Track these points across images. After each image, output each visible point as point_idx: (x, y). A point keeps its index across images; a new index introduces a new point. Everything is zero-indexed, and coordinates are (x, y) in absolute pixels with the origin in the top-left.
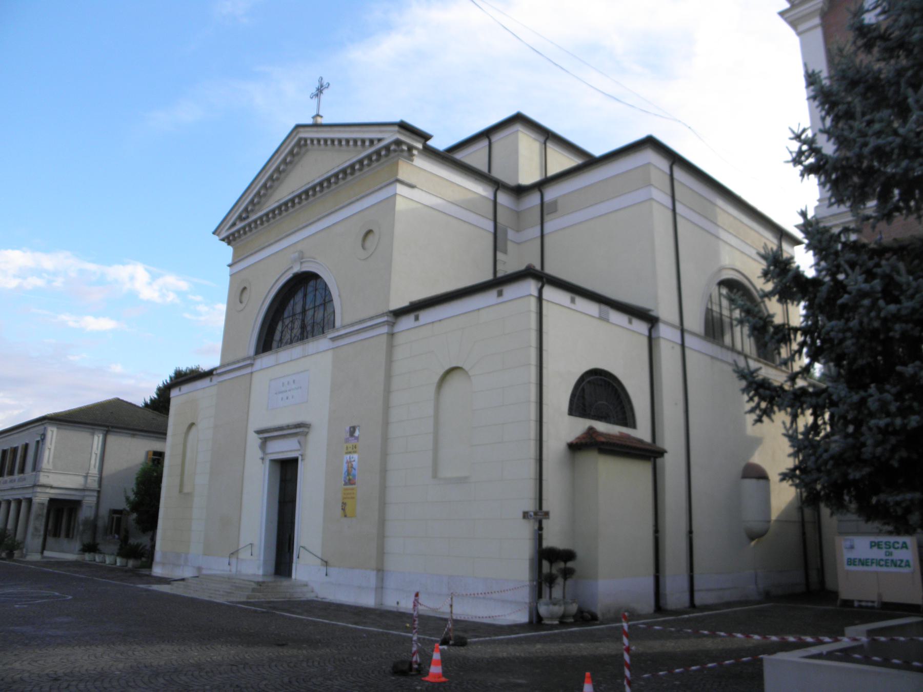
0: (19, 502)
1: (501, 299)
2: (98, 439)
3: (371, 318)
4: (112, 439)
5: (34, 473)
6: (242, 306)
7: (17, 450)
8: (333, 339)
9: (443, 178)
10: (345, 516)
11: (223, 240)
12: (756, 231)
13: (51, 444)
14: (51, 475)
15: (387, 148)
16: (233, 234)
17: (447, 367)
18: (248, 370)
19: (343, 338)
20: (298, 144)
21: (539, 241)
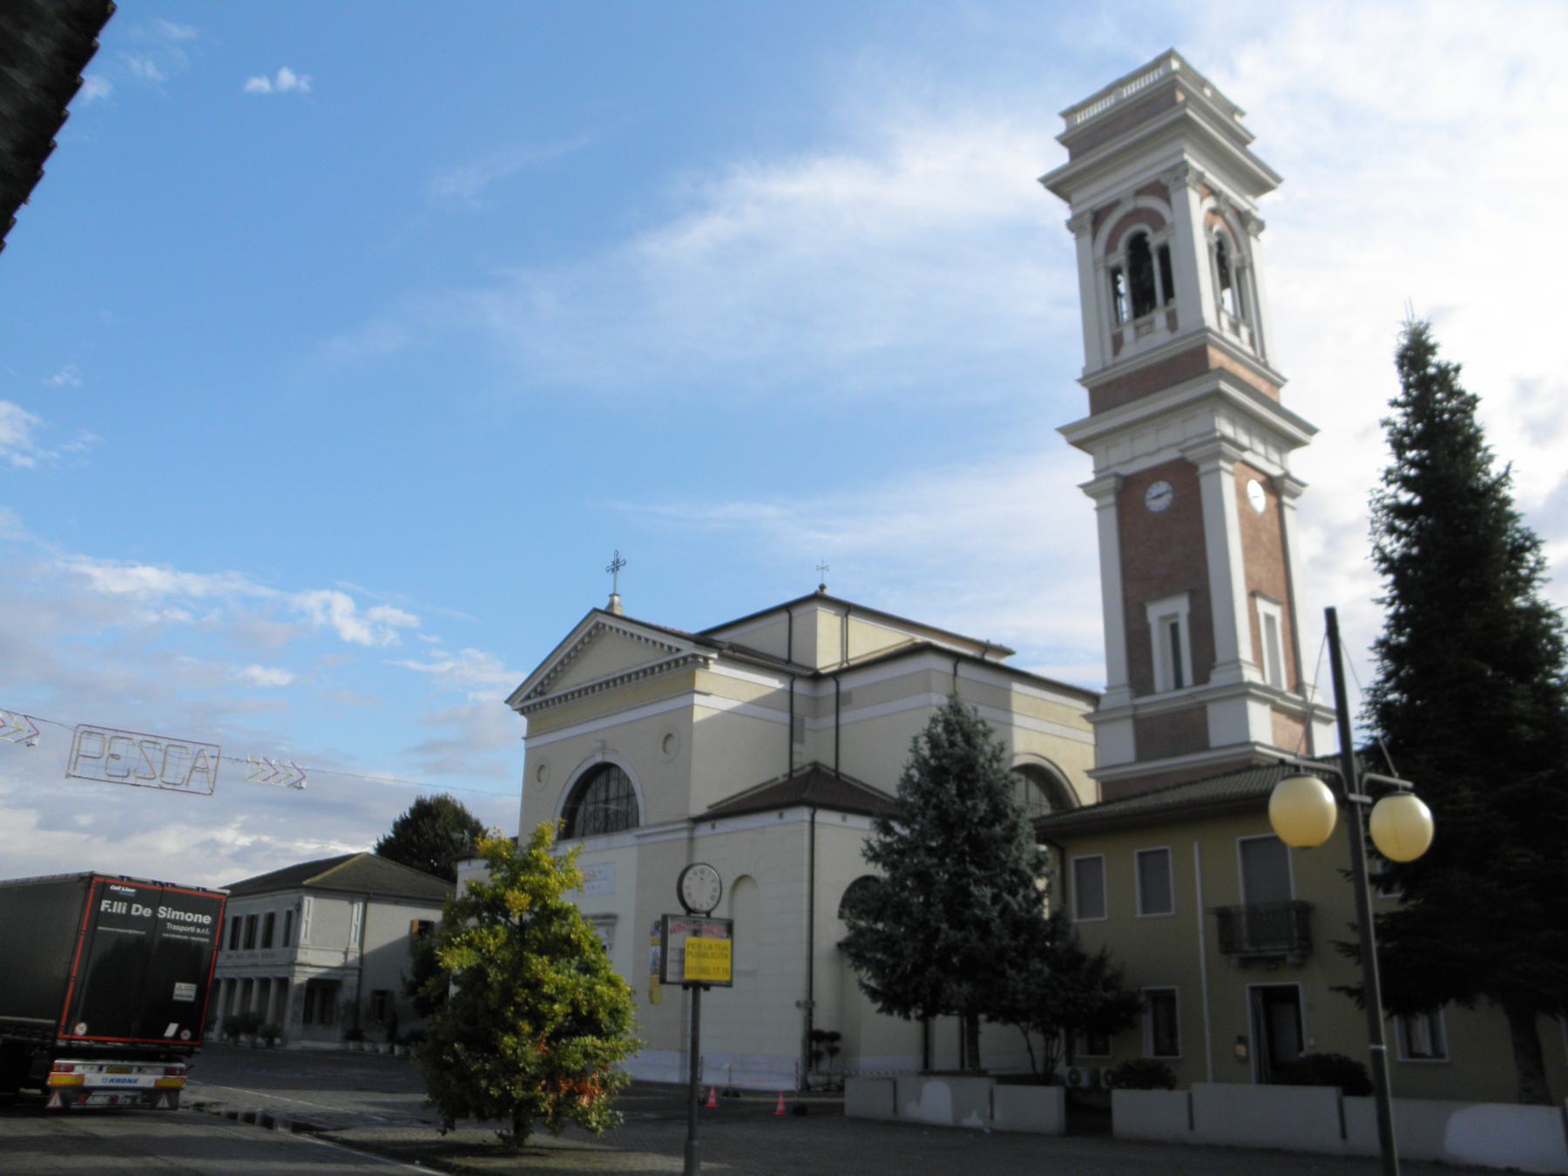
0: (265, 983)
2: (357, 908)
3: (673, 823)
4: (372, 907)
5: (288, 949)
7: (257, 920)
8: (638, 837)
9: (738, 679)
10: (652, 1002)
11: (516, 710)
12: (1063, 705)
13: (308, 916)
14: (310, 952)
15: (685, 659)
16: (528, 707)
17: (738, 875)
20: (597, 626)
21: (833, 731)
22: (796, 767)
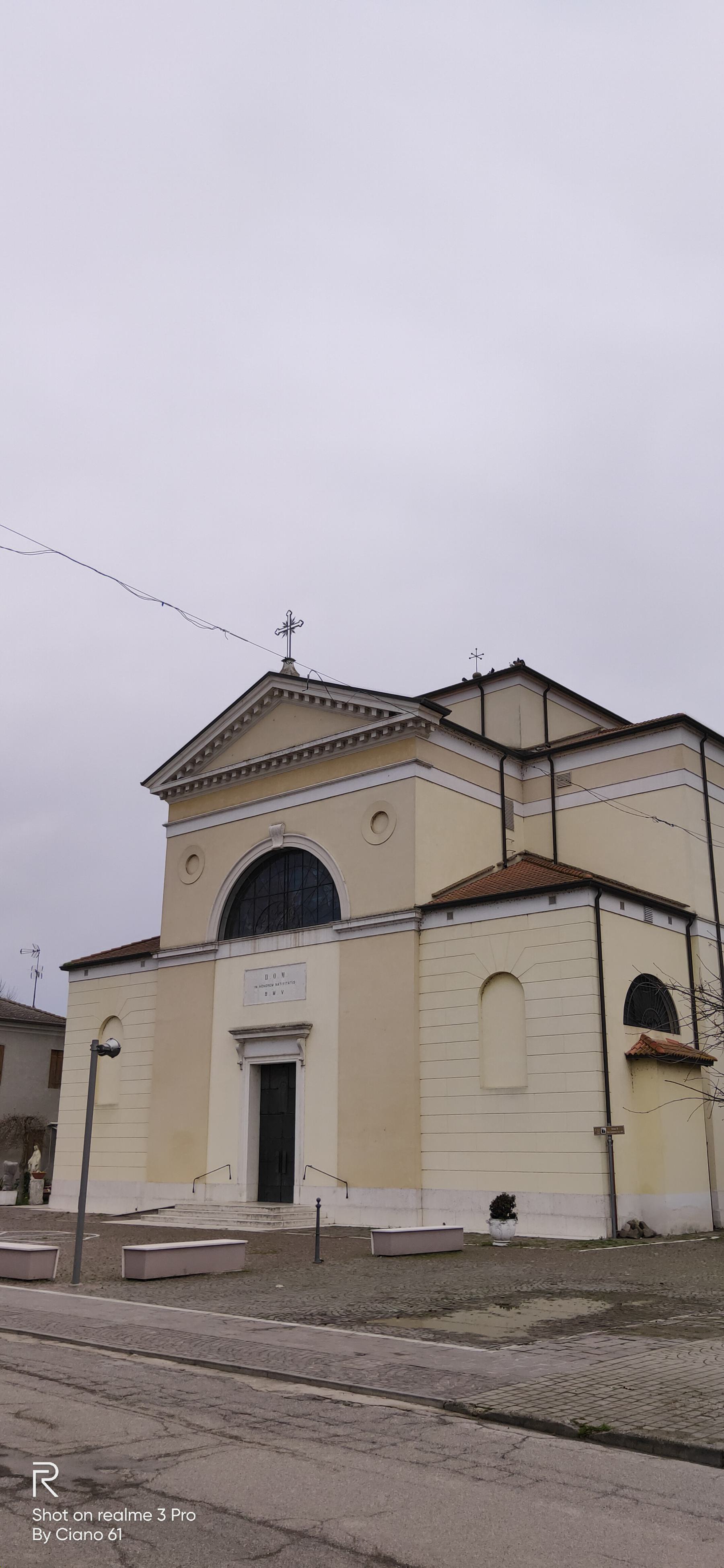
1: (553, 907)
6: (189, 879)
8: (339, 931)
11: (157, 793)
15: (403, 724)
16: (174, 790)
18: (211, 957)
19: (354, 931)
20: (270, 694)
22: (509, 855)
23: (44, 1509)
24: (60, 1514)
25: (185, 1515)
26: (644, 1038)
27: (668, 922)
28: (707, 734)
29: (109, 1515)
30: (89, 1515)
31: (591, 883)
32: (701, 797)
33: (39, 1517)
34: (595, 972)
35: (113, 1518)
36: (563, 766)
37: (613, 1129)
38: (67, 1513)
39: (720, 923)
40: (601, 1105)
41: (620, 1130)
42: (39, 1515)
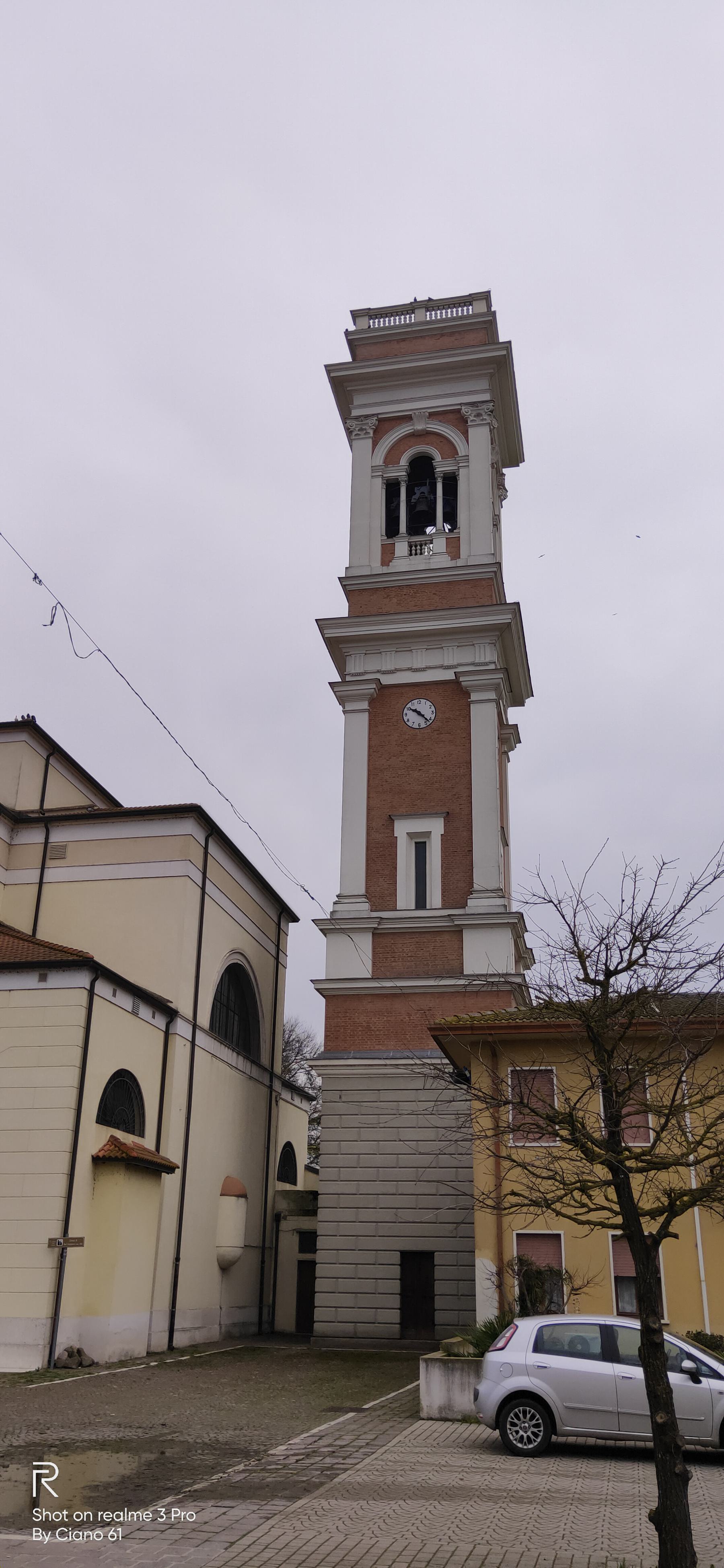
1: (42, 985)
23: (44, 1509)
24: (60, 1514)
25: (185, 1515)
26: (113, 1140)
27: (151, 1015)
28: (214, 830)
29: (109, 1515)
30: (89, 1515)
31: (91, 963)
32: (198, 891)
33: (39, 1517)
34: (78, 1062)
35: (112, 1518)
36: (59, 836)
37: (71, 1241)
38: (67, 1513)
39: (198, 1023)
40: (60, 1214)
41: (79, 1242)
42: (39, 1515)
